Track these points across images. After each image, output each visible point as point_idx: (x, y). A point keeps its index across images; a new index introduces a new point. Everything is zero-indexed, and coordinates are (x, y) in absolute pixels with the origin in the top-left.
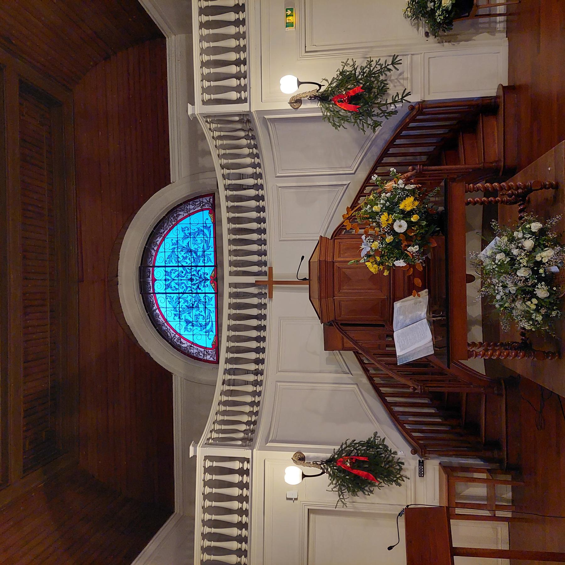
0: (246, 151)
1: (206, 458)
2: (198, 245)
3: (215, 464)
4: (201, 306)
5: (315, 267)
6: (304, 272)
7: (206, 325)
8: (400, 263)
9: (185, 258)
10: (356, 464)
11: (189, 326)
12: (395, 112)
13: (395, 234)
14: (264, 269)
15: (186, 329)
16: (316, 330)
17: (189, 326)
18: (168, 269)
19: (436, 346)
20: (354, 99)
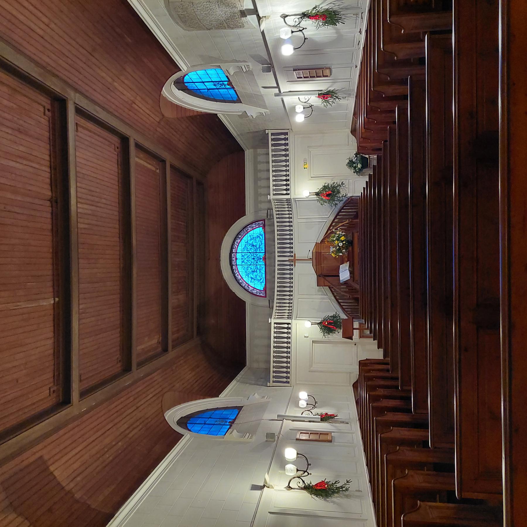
0: (287, 209)
1: (275, 323)
2: (257, 243)
3: (278, 325)
4: (258, 271)
5: (315, 254)
6: (310, 256)
7: (261, 279)
8: (341, 254)
9: (251, 249)
10: (329, 323)
11: (253, 280)
12: (342, 200)
13: (339, 246)
14: (292, 254)
15: (251, 281)
16: (314, 277)
17: (253, 280)
18: (243, 254)
19: (351, 277)
20: (328, 195)
